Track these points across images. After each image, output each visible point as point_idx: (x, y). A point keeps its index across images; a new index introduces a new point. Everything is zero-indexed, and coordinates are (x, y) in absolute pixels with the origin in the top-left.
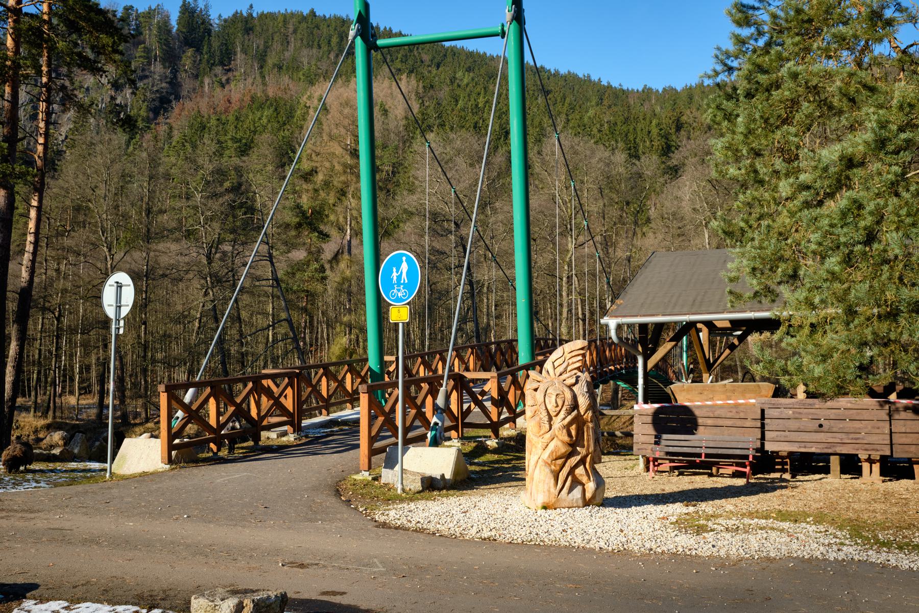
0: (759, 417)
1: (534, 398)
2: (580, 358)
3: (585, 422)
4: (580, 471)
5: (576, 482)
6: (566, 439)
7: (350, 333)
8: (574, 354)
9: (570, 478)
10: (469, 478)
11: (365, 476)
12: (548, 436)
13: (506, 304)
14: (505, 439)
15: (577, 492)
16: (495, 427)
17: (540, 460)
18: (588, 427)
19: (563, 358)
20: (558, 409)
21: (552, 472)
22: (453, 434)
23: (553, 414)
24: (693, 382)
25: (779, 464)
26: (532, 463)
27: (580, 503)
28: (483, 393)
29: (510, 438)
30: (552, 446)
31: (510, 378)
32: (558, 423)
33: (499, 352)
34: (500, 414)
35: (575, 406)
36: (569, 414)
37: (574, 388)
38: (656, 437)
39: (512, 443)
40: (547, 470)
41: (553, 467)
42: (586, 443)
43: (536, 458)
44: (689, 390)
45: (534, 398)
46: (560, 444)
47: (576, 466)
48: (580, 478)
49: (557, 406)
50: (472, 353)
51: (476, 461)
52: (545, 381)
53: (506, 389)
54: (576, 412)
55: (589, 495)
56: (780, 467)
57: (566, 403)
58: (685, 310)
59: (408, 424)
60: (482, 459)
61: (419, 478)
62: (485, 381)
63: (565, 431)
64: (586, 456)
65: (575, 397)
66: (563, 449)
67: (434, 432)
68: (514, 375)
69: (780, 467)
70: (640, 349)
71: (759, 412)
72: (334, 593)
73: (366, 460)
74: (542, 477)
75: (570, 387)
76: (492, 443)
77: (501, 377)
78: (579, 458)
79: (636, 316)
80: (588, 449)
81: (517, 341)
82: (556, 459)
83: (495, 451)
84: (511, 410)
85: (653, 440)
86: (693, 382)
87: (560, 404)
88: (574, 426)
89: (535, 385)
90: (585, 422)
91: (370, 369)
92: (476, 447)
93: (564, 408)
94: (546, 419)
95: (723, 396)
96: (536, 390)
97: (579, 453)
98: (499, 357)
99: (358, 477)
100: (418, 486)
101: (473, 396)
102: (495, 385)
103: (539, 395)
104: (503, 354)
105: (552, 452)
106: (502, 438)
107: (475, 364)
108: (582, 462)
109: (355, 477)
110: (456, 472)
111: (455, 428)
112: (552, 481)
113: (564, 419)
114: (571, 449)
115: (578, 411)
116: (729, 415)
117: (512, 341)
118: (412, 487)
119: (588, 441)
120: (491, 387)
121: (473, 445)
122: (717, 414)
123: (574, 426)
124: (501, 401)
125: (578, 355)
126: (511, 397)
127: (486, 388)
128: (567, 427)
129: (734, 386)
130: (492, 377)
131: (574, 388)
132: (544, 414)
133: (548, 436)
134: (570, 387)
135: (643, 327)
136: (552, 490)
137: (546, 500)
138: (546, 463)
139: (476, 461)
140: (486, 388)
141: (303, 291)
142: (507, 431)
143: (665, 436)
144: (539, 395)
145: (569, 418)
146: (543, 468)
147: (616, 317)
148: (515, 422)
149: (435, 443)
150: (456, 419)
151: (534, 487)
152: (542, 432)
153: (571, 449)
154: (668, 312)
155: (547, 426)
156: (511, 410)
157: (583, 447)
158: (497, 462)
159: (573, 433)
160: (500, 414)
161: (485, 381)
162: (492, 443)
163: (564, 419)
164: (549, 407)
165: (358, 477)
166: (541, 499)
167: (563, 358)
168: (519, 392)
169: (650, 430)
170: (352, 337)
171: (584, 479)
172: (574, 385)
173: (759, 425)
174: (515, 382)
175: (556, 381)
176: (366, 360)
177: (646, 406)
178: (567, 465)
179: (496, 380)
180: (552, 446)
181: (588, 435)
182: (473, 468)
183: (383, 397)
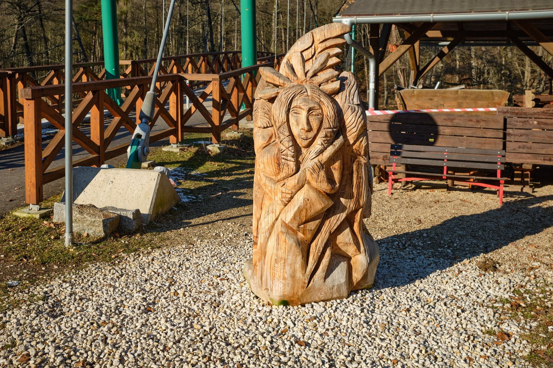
0: (502, 127)
1: (268, 113)
2: (338, 50)
3: (354, 156)
4: (345, 238)
5: (339, 256)
6: (325, 187)
7: (127, 49)
8: (328, 43)
9: (328, 252)
10: (181, 206)
11: (32, 211)
12: (292, 182)
13: (233, 30)
14: (227, 142)
15: (339, 275)
16: (217, 131)
17: (279, 223)
18: (359, 164)
19: (311, 50)
20: (311, 135)
21: (299, 243)
22: (172, 138)
23: (302, 143)
24: (424, 87)
25: (518, 176)
26: (265, 224)
27: (344, 290)
28: (204, 96)
29: (233, 141)
30: (300, 198)
31: (232, 80)
32: (310, 159)
33: (226, 61)
34: (221, 118)
35: (340, 129)
36: (330, 143)
37: (338, 98)
38: (392, 147)
39: (234, 147)
40: (291, 242)
41: (300, 235)
42: (355, 191)
43: (271, 218)
44: (419, 96)
45: (268, 113)
46: (313, 195)
47: (339, 230)
48: (344, 249)
49: (310, 130)
50: (204, 60)
51: (193, 173)
52: (288, 85)
53: (229, 92)
54: (341, 139)
55: (357, 276)
56: (519, 179)
57: (326, 124)
58: (425, 10)
59: (107, 134)
60: (202, 170)
61: (99, 220)
62: (206, 84)
63: (322, 173)
64: (356, 211)
65: (339, 114)
66: (319, 205)
67: (134, 148)
68: (237, 77)
69: (519, 179)
70: (372, 51)
71: (502, 121)
72: (125, 210)
73: (34, 191)
74: (281, 253)
75: (331, 95)
76: (214, 148)
77: (223, 79)
78: (343, 215)
79: (373, 15)
80: (358, 201)
81: (240, 52)
82: (307, 222)
83: (216, 158)
84: (234, 112)
85: (388, 149)
86: (424, 87)
87: (315, 124)
88: (337, 165)
89: (270, 92)
90: (354, 156)
91: (106, 72)
92: (196, 153)
93: (322, 134)
94: (290, 152)
95: (454, 103)
96: (272, 100)
97: (344, 208)
98: (223, 62)
99: (21, 213)
100: (98, 231)
101: (193, 100)
102: (217, 87)
103: (278, 111)
104: (229, 62)
105: (300, 211)
106: (223, 142)
107: (206, 68)
108: (349, 222)
109: (18, 213)
110: (158, 202)
111: (174, 132)
112: (299, 259)
113: (321, 152)
114: (331, 203)
115: (345, 137)
116: (469, 124)
117: (237, 52)
118: (91, 232)
119: (359, 187)
120: (213, 89)
121: (194, 150)
122: (456, 122)
123: (337, 165)
124: (224, 104)
125: (336, 46)
126: (234, 100)
127: (208, 91)
128: (326, 167)
129: (467, 93)
130: (214, 79)
131: (338, 98)
132: (287, 143)
133: (292, 182)
134: (331, 95)
135: (374, 26)
136: (299, 274)
137: (288, 291)
138: (286, 226)
139: (193, 173)
140: (208, 91)
141: (93, 20)
142: (229, 134)
143: (406, 147)
144: (278, 111)
145: (330, 150)
146: (283, 237)
147: (350, 15)
148: (237, 124)
149: (135, 163)
150: (175, 123)
151: (266, 267)
152: (283, 175)
153: (331, 203)
154: (407, 10)
155: (292, 165)
156: (234, 112)
157: (351, 197)
158: (217, 173)
159: (336, 175)
160: (221, 118)
161: (206, 84)
162: (214, 148)
163: (321, 152)
164: (295, 131)
165: (21, 213)
166: (278, 290)
167: (311, 50)
168: (242, 94)
169: (387, 138)
170: (128, 52)
171: (350, 250)
172: (337, 92)
173: (501, 135)
174: (238, 84)
175: (307, 86)
176: (103, 64)
177: (378, 113)
178: (324, 229)
179: (217, 83)
180: (300, 198)
181: (359, 178)
182: (189, 185)
183: (119, 97)
